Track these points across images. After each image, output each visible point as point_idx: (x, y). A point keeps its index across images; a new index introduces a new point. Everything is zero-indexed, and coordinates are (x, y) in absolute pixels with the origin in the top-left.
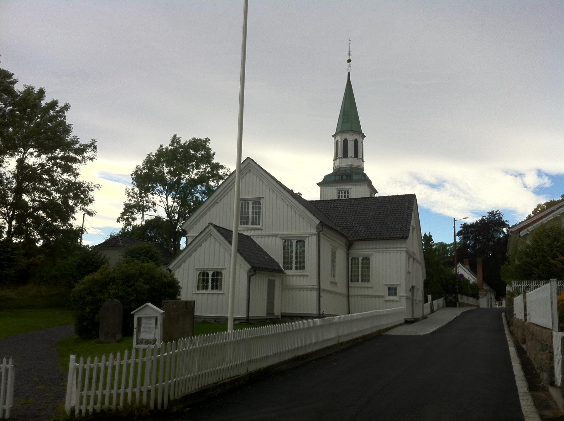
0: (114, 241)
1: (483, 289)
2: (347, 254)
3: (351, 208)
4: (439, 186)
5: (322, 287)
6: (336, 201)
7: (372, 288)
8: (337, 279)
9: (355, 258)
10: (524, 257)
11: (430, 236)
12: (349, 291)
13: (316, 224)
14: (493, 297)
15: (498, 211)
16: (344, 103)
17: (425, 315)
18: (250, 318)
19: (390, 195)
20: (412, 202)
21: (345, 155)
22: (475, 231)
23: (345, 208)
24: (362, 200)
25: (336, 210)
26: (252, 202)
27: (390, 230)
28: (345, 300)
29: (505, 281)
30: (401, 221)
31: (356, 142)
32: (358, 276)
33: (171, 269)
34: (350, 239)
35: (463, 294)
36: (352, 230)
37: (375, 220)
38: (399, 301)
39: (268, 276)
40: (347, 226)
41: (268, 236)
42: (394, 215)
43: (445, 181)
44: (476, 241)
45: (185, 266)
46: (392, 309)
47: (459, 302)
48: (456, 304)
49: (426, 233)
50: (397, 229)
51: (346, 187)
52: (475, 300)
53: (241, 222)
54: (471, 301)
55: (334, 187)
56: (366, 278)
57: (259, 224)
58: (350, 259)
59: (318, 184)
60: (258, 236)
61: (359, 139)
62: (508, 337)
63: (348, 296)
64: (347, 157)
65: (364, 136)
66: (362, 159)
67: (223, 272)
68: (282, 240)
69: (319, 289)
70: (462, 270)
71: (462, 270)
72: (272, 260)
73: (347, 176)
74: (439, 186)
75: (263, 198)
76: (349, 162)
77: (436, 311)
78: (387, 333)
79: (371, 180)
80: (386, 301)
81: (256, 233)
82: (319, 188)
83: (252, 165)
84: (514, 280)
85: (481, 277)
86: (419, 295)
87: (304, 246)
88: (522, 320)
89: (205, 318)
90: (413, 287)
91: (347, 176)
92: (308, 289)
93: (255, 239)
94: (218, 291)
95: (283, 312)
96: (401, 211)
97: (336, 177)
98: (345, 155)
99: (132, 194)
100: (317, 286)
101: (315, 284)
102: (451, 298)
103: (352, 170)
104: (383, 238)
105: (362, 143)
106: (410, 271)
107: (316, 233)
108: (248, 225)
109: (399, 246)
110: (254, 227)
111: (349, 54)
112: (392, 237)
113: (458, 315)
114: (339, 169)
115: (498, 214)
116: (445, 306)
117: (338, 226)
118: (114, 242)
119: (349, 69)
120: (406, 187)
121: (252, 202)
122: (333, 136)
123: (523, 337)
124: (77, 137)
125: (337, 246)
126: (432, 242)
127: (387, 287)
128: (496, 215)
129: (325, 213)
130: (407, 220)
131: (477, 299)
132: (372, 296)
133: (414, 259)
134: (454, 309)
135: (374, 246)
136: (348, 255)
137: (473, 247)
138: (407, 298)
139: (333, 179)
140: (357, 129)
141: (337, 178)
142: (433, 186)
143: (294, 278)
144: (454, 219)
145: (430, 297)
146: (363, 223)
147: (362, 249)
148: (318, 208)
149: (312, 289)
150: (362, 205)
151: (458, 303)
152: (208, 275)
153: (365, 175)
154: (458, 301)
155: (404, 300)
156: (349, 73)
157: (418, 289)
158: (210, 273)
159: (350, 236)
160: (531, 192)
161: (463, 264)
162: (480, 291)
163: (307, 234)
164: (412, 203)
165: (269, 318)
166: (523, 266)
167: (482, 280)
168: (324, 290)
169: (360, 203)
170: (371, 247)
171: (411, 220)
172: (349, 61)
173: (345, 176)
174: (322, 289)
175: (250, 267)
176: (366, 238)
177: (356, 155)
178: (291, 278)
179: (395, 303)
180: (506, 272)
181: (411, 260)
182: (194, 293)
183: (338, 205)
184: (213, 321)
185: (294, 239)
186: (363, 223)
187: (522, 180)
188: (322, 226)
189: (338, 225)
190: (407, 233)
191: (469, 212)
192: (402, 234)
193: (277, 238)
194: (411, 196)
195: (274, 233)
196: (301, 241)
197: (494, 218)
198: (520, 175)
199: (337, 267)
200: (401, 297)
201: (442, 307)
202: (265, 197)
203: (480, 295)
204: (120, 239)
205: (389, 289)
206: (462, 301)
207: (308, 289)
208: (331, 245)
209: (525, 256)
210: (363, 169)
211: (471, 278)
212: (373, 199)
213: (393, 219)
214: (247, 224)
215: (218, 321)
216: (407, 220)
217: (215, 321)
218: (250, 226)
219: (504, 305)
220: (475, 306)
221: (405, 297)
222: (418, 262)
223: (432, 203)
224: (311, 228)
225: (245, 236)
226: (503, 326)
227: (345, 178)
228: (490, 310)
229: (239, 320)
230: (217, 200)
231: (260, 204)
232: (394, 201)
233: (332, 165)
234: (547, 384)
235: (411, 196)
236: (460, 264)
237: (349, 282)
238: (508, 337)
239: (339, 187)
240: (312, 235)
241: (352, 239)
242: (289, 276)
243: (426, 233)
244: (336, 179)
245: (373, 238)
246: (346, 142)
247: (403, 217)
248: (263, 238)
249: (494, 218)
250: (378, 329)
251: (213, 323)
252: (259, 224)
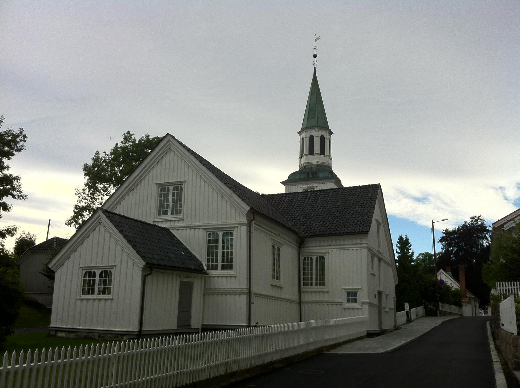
0: (48, 244)
1: (467, 297)
2: (298, 253)
3: (306, 201)
4: (423, 199)
5: (254, 290)
6: (291, 195)
7: (328, 292)
8: (282, 282)
9: (308, 258)
10: (510, 254)
11: (407, 239)
12: (300, 298)
13: (246, 211)
14: (477, 305)
15: (480, 216)
16: (310, 98)
17: (398, 326)
18: (143, 333)
19: (351, 186)
20: (375, 193)
21: (311, 152)
22: (457, 238)
23: (300, 202)
24: (320, 192)
25: (290, 204)
26: (173, 187)
27: (348, 224)
28: (296, 307)
29: (487, 283)
30: (362, 213)
31: (322, 138)
32: (311, 279)
33: (52, 267)
34: (301, 235)
35: (443, 302)
36: (305, 225)
37: (332, 213)
38: (361, 308)
39: (180, 277)
40: (301, 220)
41: (190, 228)
42: (354, 207)
43: (429, 195)
44: (460, 248)
45: (69, 264)
46: (344, 318)
47: (440, 311)
48: (437, 312)
49: (401, 235)
50: (357, 222)
51: (311, 185)
52: (458, 308)
53: (160, 212)
54: (454, 309)
55: (299, 186)
56: (321, 282)
57: (180, 213)
58: (302, 259)
59: (282, 183)
60: (178, 228)
61: (326, 135)
62: (494, 355)
63: (300, 303)
64: (314, 154)
65: (331, 133)
66: (330, 156)
67: (113, 271)
68: (207, 232)
69: (249, 293)
70: (444, 276)
71: (444, 276)
72: (193, 258)
73: (313, 174)
74: (423, 199)
75: (185, 181)
76: (316, 159)
77: (414, 320)
78: (333, 352)
79: (340, 179)
80: (345, 309)
81: (176, 224)
82: (284, 187)
83: (173, 144)
84: (500, 282)
85: (464, 284)
86: (390, 302)
87: (232, 239)
88: (513, 334)
89: (88, 333)
90: (380, 293)
91: (313, 174)
92: (235, 293)
93: (174, 232)
94: (106, 297)
95: (206, 323)
96: (362, 203)
97: (301, 175)
98: (311, 152)
99: (83, 195)
100: (247, 289)
101: (244, 287)
102: (431, 306)
103: (318, 167)
104: (339, 233)
105: (329, 139)
106: (374, 273)
107: (247, 222)
108: (168, 215)
109: (359, 242)
110: (175, 217)
112: (349, 231)
113: (437, 325)
114: (305, 166)
115: (480, 219)
116: (425, 315)
117: (290, 221)
118: (48, 245)
119: (315, 64)
120: (392, 201)
121: (173, 187)
122: (299, 133)
123: (515, 360)
124: (12, 130)
125: (282, 243)
126: (409, 245)
127: (346, 292)
128: (479, 221)
129: (279, 209)
130: (368, 213)
131: (460, 308)
132: (328, 303)
133: (380, 260)
134: (436, 318)
135: (330, 243)
136: (299, 254)
137: (456, 254)
138: (370, 305)
139: (298, 177)
140: (323, 125)
141: (302, 176)
142: (418, 200)
143: (220, 279)
144: (432, 220)
145: (407, 305)
146: (318, 217)
147: (315, 247)
148: (271, 202)
149: (240, 293)
150: (320, 198)
151: (438, 312)
152: (95, 275)
153: (332, 173)
154: (438, 309)
155: (366, 307)
156: (315, 68)
157: (387, 296)
158: (98, 273)
159: (302, 232)
160: (512, 205)
161: (445, 270)
162: (463, 299)
163: (235, 224)
164: (376, 194)
165: (179, 332)
166: (510, 265)
167: (465, 287)
168: (258, 295)
169: (318, 196)
170: (326, 244)
171: (373, 213)
172: (315, 56)
173: (310, 174)
174: (254, 294)
175: (144, 263)
176: (320, 234)
177: (323, 152)
178: (216, 279)
179: (356, 311)
180: (489, 273)
181: (376, 260)
182: (78, 299)
183: (293, 199)
184: (97, 335)
185: (220, 231)
186: (318, 217)
187: (503, 193)
188: (253, 214)
189: (290, 220)
190: (367, 227)
191: (454, 224)
192: (361, 228)
193: (201, 230)
194: (375, 187)
195: (197, 223)
196: (228, 233)
197: (476, 224)
198: (501, 188)
200: (364, 303)
201: (421, 317)
202: (187, 181)
203: (463, 304)
204: (55, 241)
205: (349, 294)
206: (444, 310)
207: (235, 293)
208: (272, 239)
209: (511, 252)
210: (330, 167)
211: (453, 285)
212: (332, 191)
213: (352, 212)
214: (167, 214)
215: (103, 337)
216: (368, 213)
217: (100, 336)
218: (170, 216)
219: (490, 313)
220: (458, 314)
221: (368, 303)
222: (386, 262)
223: (418, 216)
224: (240, 217)
225: (134, 222)
226: (487, 338)
227: (311, 176)
228: (475, 319)
229: (128, 335)
230: (132, 186)
231: (181, 189)
232: (355, 193)
235: (375, 187)
236: (441, 270)
238: (494, 355)
239: (304, 186)
240: (241, 224)
241: (304, 235)
242: (214, 277)
243: (401, 235)
244: (302, 177)
245: (328, 234)
247: (364, 210)
248: (184, 230)
249: (476, 224)
250: (319, 346)
251: (97, 338)
252: (180, 213)
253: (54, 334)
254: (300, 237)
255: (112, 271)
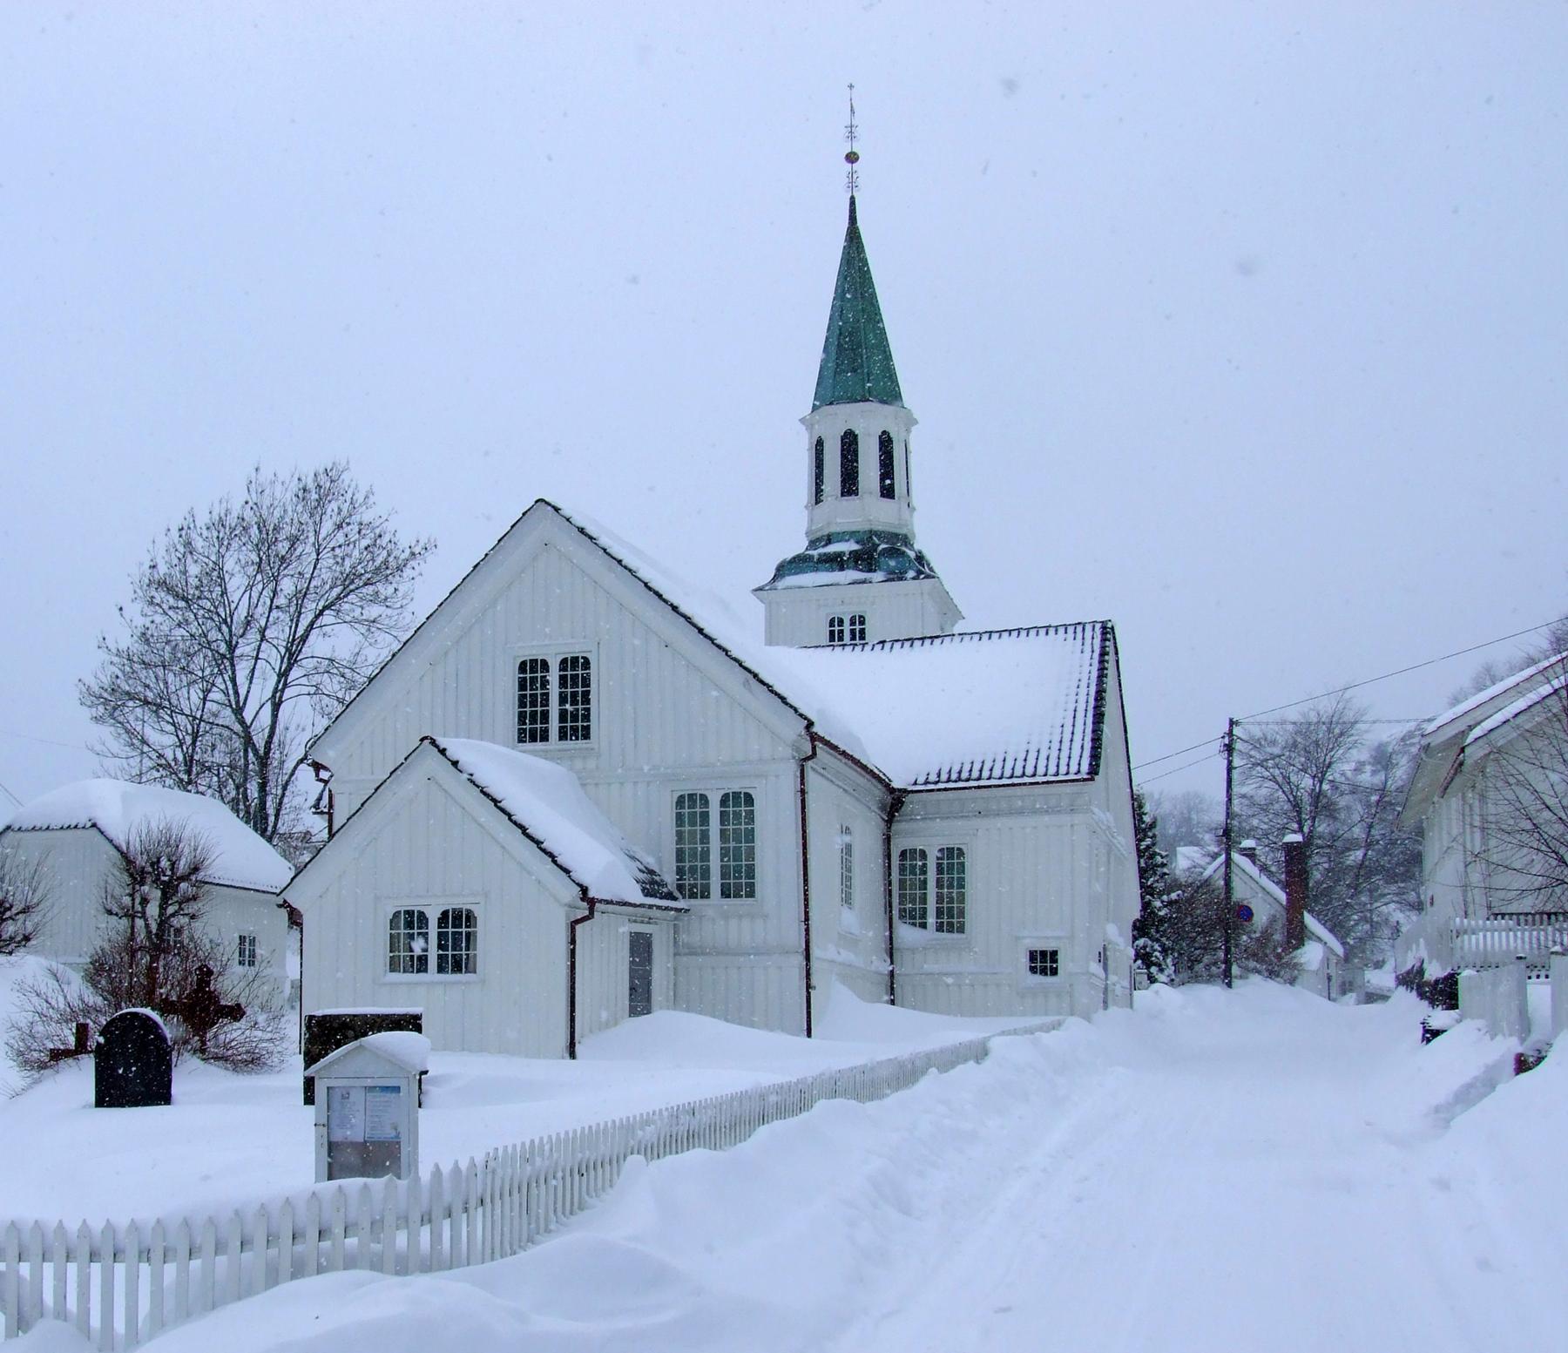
21: (850, 484)
53: (521, 732)
56: (951, 920)
76: (869, 511)
111: (852, 136)
119: (852, 185)
136: (888, 840)
172: (852, 158)
177: (888, 492)
199: (856, 882)
233: (803, 525)
234: (1489, 850)
237: (891, 919)
246: (850, 443)
253: (423, 1077)
254: (892, 791)
255: (425, 912)
